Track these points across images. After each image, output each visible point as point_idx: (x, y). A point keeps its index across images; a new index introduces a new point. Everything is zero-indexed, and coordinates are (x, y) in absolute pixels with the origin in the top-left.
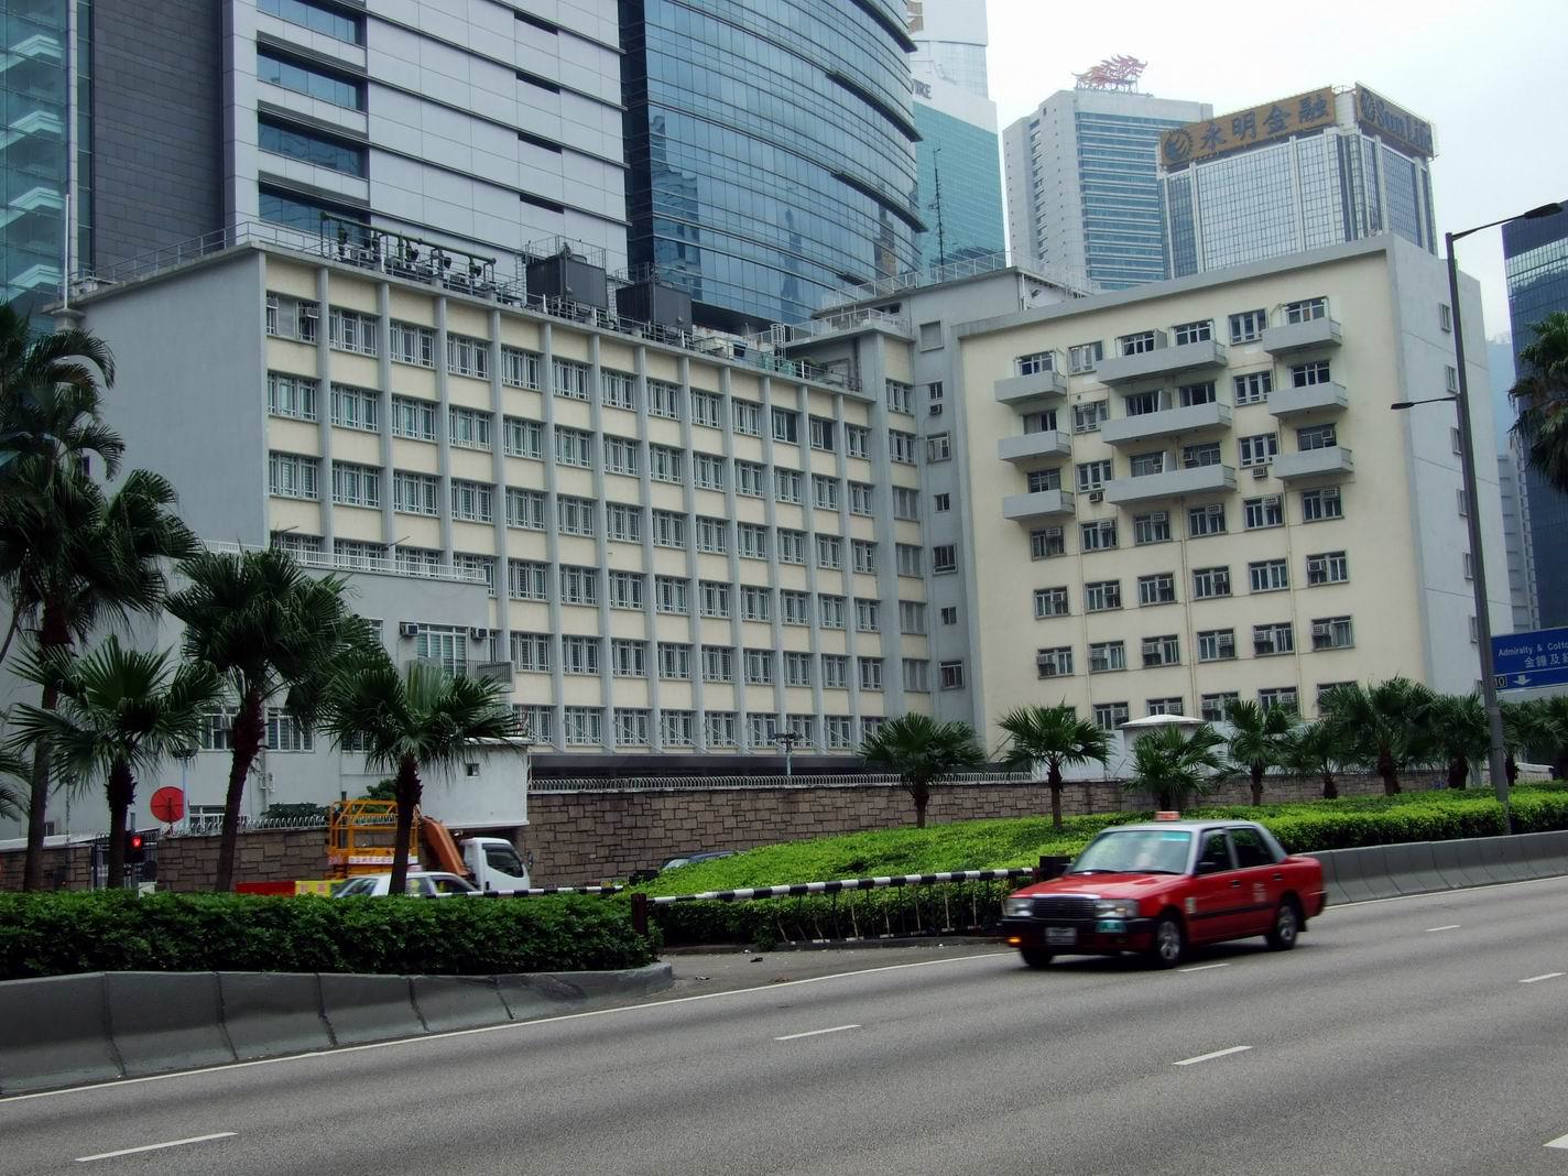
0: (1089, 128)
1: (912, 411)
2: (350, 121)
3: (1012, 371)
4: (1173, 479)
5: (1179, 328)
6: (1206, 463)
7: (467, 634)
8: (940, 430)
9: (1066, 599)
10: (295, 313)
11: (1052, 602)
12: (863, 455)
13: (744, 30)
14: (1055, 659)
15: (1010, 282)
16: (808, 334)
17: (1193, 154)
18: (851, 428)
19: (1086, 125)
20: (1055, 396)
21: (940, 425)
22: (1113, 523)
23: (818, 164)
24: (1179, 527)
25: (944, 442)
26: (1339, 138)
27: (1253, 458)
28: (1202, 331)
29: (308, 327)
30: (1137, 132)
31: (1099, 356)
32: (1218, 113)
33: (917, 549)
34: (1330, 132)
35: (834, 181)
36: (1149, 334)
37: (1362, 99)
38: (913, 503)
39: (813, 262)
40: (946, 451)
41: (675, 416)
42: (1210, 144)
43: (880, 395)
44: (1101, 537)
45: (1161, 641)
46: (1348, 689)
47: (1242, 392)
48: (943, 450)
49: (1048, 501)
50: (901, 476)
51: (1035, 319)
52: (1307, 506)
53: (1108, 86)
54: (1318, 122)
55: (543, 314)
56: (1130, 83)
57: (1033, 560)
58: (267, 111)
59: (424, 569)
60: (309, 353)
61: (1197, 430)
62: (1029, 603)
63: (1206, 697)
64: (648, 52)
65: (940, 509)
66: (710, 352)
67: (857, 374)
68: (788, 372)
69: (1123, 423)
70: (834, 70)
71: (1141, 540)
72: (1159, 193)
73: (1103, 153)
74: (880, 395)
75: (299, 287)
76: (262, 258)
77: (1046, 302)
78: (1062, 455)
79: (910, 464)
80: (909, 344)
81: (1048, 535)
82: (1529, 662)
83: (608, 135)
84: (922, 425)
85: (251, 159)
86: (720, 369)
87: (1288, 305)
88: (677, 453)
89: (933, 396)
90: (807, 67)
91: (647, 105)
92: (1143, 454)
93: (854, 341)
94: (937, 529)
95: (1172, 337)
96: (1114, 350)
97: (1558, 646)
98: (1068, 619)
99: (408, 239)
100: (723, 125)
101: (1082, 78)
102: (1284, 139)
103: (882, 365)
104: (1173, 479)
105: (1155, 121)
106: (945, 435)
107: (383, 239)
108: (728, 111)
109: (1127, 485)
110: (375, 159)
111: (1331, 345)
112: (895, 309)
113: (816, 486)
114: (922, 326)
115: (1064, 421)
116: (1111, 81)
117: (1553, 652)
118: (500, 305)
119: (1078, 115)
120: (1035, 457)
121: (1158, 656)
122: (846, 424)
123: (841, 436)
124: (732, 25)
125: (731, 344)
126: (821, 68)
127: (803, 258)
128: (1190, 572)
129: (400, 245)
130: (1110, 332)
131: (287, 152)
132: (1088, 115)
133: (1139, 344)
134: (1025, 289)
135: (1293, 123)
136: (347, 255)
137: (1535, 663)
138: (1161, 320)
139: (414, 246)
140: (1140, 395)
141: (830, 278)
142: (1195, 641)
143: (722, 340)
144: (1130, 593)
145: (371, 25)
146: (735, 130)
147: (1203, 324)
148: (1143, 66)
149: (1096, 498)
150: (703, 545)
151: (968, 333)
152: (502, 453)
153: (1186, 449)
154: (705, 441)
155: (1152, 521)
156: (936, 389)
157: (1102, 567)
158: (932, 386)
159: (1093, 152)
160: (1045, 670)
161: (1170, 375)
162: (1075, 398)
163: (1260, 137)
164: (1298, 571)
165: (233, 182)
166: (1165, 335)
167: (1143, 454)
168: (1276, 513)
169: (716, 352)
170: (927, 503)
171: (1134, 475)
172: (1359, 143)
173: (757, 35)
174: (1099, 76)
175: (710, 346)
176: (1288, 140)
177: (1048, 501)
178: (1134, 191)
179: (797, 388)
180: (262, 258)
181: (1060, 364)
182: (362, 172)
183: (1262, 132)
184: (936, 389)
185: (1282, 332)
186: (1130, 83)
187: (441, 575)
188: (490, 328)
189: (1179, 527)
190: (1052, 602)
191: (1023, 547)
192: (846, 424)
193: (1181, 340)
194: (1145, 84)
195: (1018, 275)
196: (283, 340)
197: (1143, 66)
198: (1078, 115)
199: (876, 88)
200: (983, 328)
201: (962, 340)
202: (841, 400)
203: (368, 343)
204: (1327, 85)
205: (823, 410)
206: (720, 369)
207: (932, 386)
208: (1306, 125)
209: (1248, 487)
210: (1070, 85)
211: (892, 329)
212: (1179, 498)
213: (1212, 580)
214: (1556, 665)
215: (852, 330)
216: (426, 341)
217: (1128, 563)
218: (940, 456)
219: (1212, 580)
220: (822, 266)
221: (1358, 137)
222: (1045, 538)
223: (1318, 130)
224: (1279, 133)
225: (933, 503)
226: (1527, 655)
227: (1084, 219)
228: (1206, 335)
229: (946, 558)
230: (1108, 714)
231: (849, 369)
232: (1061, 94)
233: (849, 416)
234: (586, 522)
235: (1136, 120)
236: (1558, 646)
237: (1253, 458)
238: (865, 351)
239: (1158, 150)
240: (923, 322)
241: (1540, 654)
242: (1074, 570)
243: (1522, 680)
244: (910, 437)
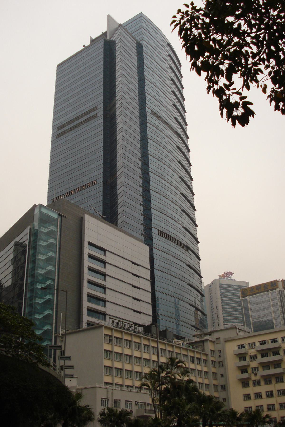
0: (222, 287)
1: (215, 356)
2: (103, 296)
3: (236, 348)
4: (272, 371)
5: (271, 340)
6: (278, 368)
7: (146, 404)
8: (221, 360)
9: (250, 396)
10: (108, 338)
11: (247, 397)
12: (139, 350)
13: (173, 276)
14: (271, 407)
15: (234, 330)
16: (193, 340)
17: (248, 294)
18: (204, 360)
19: (222, 286)
20: (246, 353)
21: (221, 359)
23: (187, 303)
24: (274, 381)
25: (222, 363)
26: (279, 291)
28: (275, 340)
29: (110, 340)
30: (233, 288)
31: (255, 345)
32: (251, 285)
33: (217, 385)
34: (277, 289)
35: (189, 306)
36: (265, 341)
37: (284, 282)
38: (216, 376)
39: (182, 321)
40: (222, 365)
41: (139, 350)
42: (251, 292)
43: (209, 353)
44: (257, 383)
45: (271, 405)
46: (248, 409)
48: (221, 364)
49: (245, 376)
50: (213, 370)
51: (240, 337)
53: (226, 278)
54: (275, 287)
55: (166, 342)
56: (230, 277)
57: (243, 388)
58: (89, 294)
59: (129, 389)
60: (110, 346)
61: (276, 361)
62: (242, 398)
64: (155, 281)
65: (221, 377)
66: (178, 345)
67: (204, 348)
68: (191, 348)
69: (260, 359)
70: (189, 283)
71: (266, 384)
72: (241, 301)
73: (226, 292)
74: (209, 353)
75: (109, 333)
76: (103, 327)
77: (242, 334)
78: (248, 366)
79: (215, 367)
80: (213, 342)
81: (246, 383)
83: (148, 298)
84: (217, 359)
85: (86, 304)
86: (180, 348)
88: (131, 356)
89: (219, 353)
90: (184, 283)
91: (155, 291)
92: (266, 366)
93: (203, 342)
94: (221, 382)
95: (270, 341)
96: (258, 344)
98: (250, 401)
99: (124, 322)
100: (169, 295)
101: (220, 276)
102: (268, 291)
103: (209, 347)
104: (272, 371)
105: (237, 286)
106: (222, 361)
107: (120, 322)
108: (170, 292)
109: (262, 372)
110: (107, 303)
112: (210, 335)
113: (144, 361)
114: (216, 338)
115: (248, 359)
116: (226, 277)
118: (142, 336)
119: (220, 284)
120: (242, 366)
122: (168, 350)
123: (202, 361)
124: (170, 275)
125: (181, 343)
126: (187, 283)
127: (180, 321)
128: (276, 391)
129: (123, 323)
130: (257, 340)
131: (93, 303)
132: (222, 284)
133: (262, 343)
134: (238, 331)
135: (269, 288)
136: (114, 326)
138: (267, 338)
139: (125, 323)
140: (264, 353)
141: (189, 326)
142: (278, 406)
143: (180, 342)
144: (264, 395)
145: (107, 277)
146: (171, 296)
147: (276, 339)
148: (233, 274)
149: (256, 375)
150: (136, 378)
151: (226, 340)
152: (134, 364)
154: (137, 354)
155: (268, 380)
156: (220, 351)
157: (258, 389)
158: (219, 351)
159: (223, 292)
161: (270, 349)
162: (250, 354)
163: (262, 290)
165: (83, 309)
166: (268, 341)
167: (266, 366)
169: (179, 344)
170: (219, 376)
171: (263, 370)
172: (284, 292)
173: (175, 277)
174: (224, 276)
175: (178, 343)
176: (268, 291)
177: (245, 376)
178: (233, 301)
179: (194, 351)
180: (103, 327)
181: (247, 347)
182: (105, 306)
183: (263, 289)
184: (220, 351)
186: (230, 277)
187: (122, 389)
188: (166, 347)
189: (274, 381)
190: (247, 397)
191: (240, 386)
192: (168, 350)
193: (272, 342)
194: (234, 277)
195: (236, 328)
196: (106, 343)
197: (233, 274)
198: (220, 284)
199: (196, 287)
200: (230, 339)
201: (225, 341)
202: (195, 352)
203: (120, 343)
204: (276, 279)
205: (199, 356)
206: (180, 348)
207: (219, 351)
208: (272, 288)
209: (253, 378)
210: (218, 278)
211: (210, 339)
212: (273, 375)
213: (281, 392)
215: (202, 339)
216: (130, 343)
217: (263, 389)
218: (221, 366)
219: (281, 392)
220: (188, 324)
221: (283, 290)
222: (245, 383)
223: (275, 289)
224: (266, 290)
225: (220, 376)
227: (222, 307)
228: (277, 341)
229: (224, 388)
231: (202, 347)
232: (216, 280)
233: (203, 357)
234: (110, 372)
235: (233, 285)
238: (205, 344)
239: (240, 293)
240: (217, 338)
242: (252, 390)
244: (215, 361)
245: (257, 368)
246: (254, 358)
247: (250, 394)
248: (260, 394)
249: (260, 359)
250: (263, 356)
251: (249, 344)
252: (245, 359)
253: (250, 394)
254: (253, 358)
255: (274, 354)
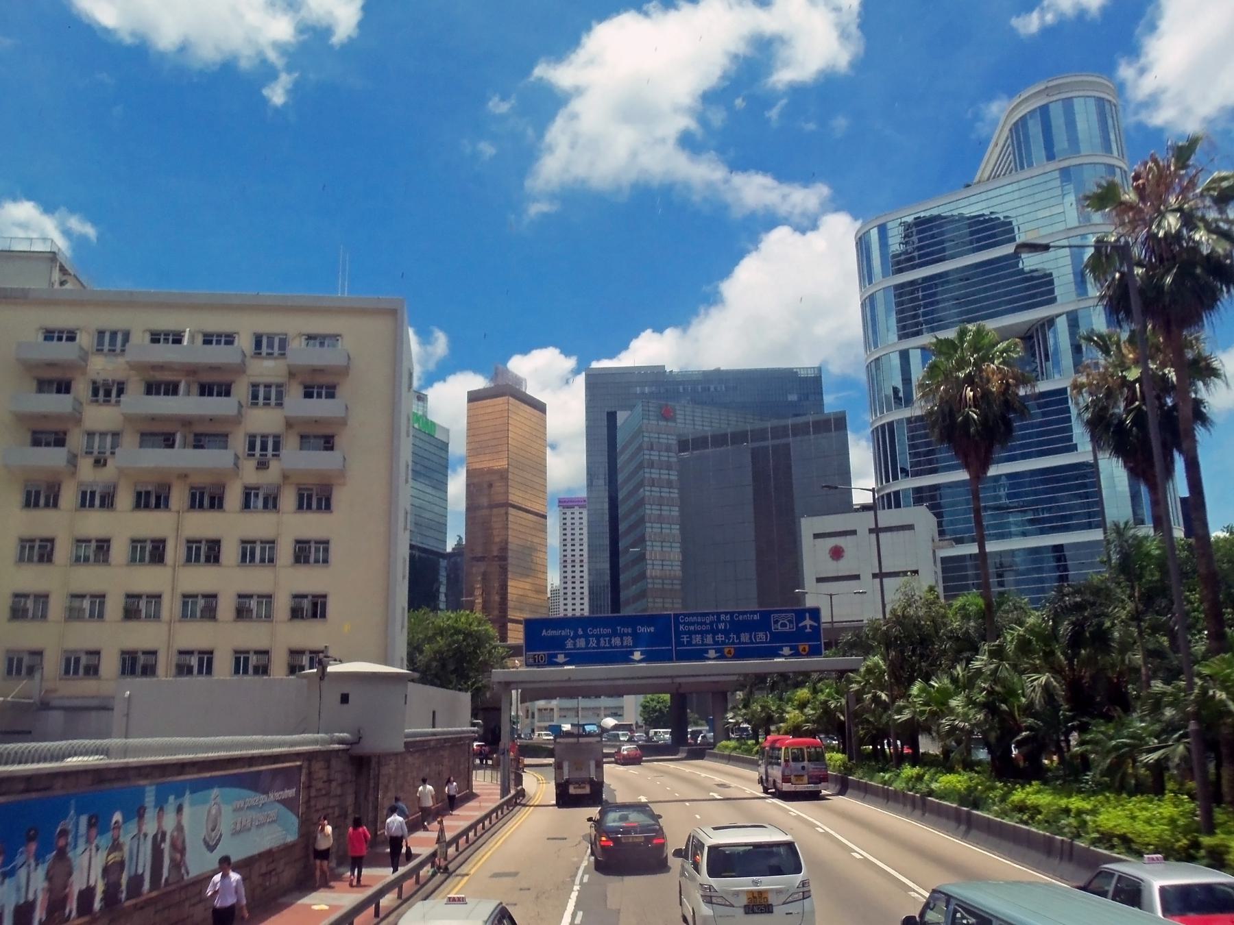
14: (30, 604)
22: (114, 488)
27: (258, 452)
47: (255, 396)
52: (301, 498)
63: (181, 653)
82: (569, 644)
87: (46, 329)
96: (139, 339)
97: (596, 631)
111: (344, 371)
117: (593, 636)
120: (45, 417)
121: (25, 611)
137: (575, 644)
153: (302, 437)
160: (18, 613)
164: (285, 552)
168: (271, 503)
185: (302, 354)
190: (305, 552)
209: (250, 474)
214: (594, 648)
226: (567, 637)
230: (246, 660)
236: (596, 631)
237: (258, 452)
241: (580, 637)
243: (561, 658)
245: (116, 435)
246: (108, 393)
247: (52, 541)
248: (49, 544)
249: (137, 403)
250: (152, 389)
251: (101, 333)
252: (64, 387)
253: (52, 541)
254: (106, 391)
255: (206, 390)
